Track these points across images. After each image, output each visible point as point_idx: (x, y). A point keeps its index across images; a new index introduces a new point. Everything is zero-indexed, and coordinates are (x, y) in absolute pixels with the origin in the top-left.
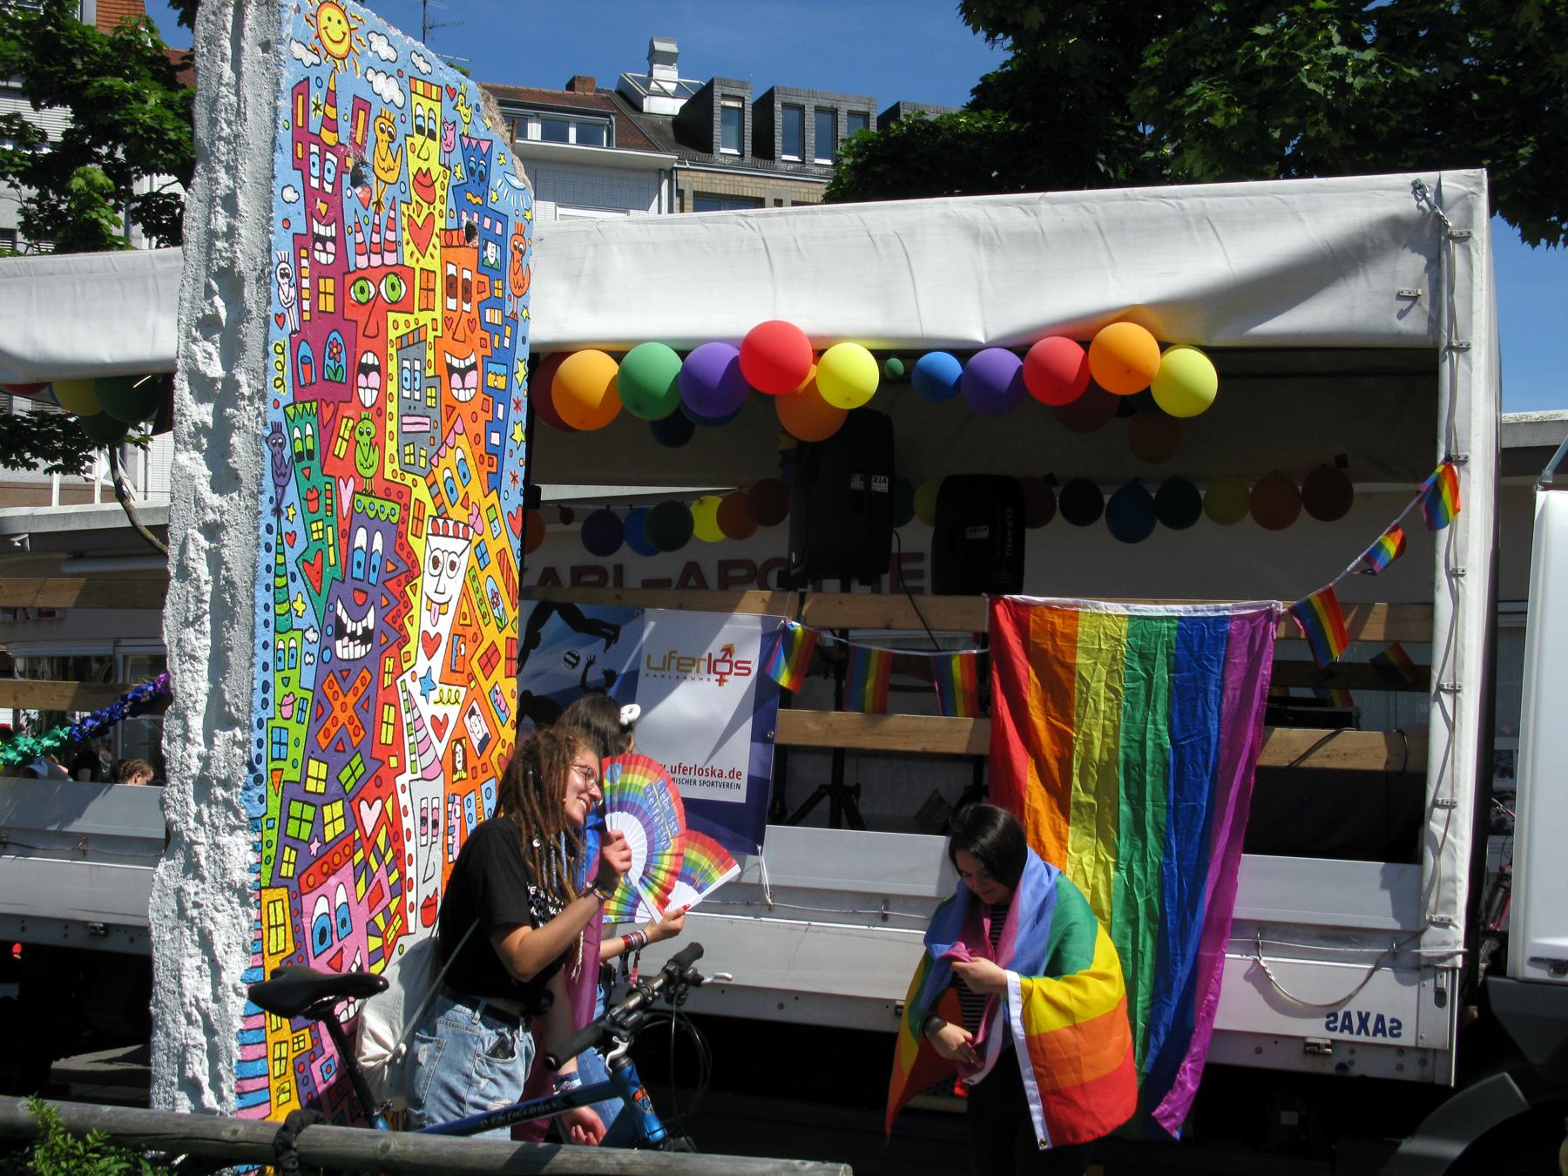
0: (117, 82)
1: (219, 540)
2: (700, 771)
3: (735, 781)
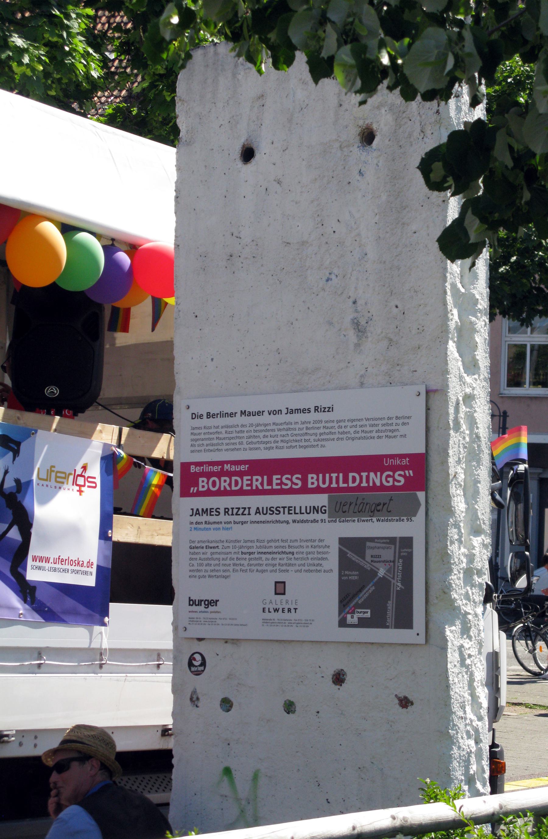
0: (494, 94)
1: (471, 407)
2: (71, 562)
3: (89, 569)
